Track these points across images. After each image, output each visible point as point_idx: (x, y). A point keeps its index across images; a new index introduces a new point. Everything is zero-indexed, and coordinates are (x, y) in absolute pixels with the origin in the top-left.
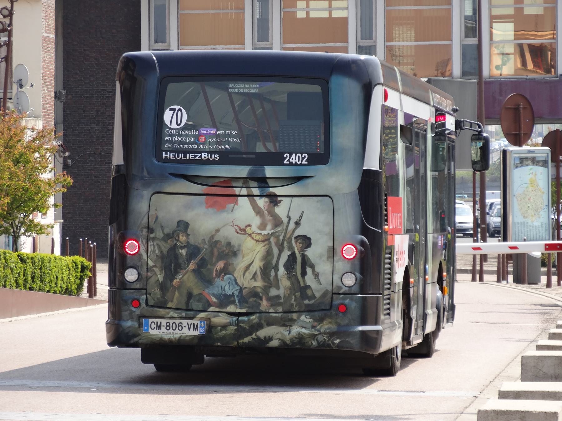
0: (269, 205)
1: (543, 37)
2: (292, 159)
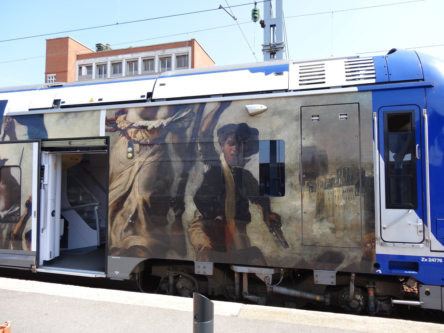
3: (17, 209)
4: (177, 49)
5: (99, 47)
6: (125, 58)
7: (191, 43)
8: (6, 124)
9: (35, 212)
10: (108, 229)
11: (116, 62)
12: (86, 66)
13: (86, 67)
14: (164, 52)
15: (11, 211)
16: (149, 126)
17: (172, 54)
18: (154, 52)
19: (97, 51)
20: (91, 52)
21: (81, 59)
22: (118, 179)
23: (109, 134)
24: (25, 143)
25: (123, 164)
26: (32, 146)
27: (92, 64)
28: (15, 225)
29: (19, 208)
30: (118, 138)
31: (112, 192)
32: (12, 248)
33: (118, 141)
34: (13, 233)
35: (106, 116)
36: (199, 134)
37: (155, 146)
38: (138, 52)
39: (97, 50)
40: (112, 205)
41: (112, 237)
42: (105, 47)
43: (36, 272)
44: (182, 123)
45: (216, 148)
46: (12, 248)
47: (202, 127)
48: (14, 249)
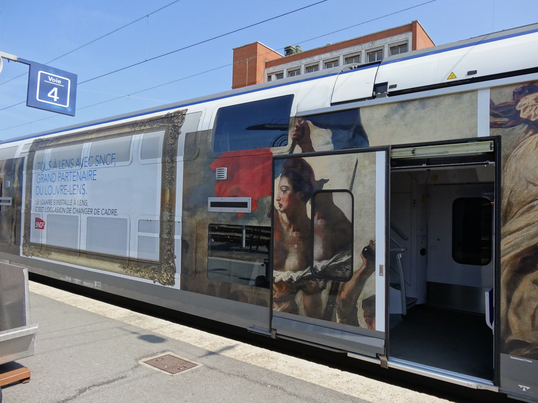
0: (290, 196)
1: (59, 141)
2: (53, 94)
3: (345, 259)
4: (392, 38)
5: (288, 50)
6: (322, 58)
7: (412, 27)
8: (295, 128)
9: (381, 267)
10: (501, 305)
11: (311, 65)
12: (276, 75)
13: (276, 75)
14: (373, 44)
15: (334, 261)
16: (276, 277)
17: (384, 46)
18: (360, 45)
19: (286, 55)
20: (280, 57)
21: (271, 66)
22: (522, 214)
23: (498, 132)
24: (359, 154)
25: (535, 186)
26: (374, 157)
27: (283, 70)
28: (344, 285)
30: (523, 137)
31: (508, 237)
33: (523, 142)
34: (340, 297)
35: (491, 100)
38: (339, 50)
39: (286, 54)
40: (509, 261)
41: (510, 321)
42: (295, 49)
43: (387, 368)
45: (361, 325)
46: (338, 320)
48: (341, 322)
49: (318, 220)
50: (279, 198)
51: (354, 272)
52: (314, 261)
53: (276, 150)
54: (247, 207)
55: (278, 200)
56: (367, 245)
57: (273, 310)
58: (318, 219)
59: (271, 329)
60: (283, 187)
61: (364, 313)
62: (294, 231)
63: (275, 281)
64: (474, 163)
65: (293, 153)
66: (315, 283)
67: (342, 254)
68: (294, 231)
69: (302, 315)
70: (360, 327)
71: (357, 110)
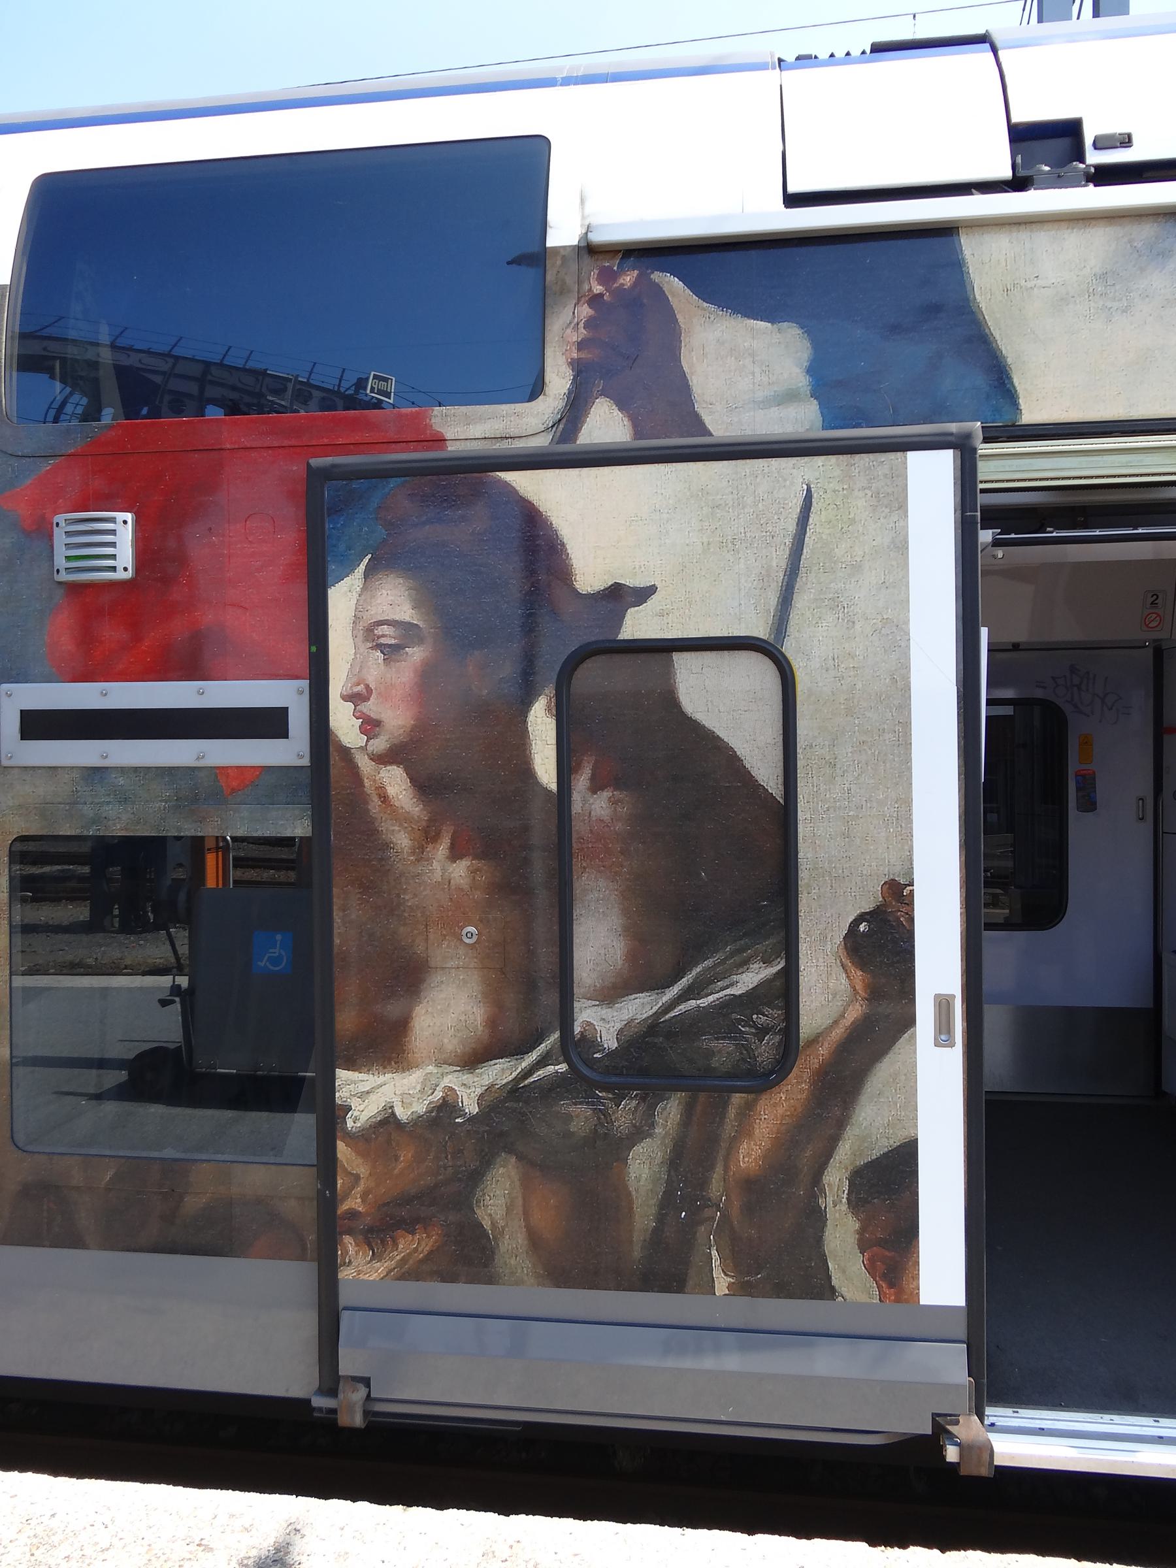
0: (427, 676)
3: (749, 979)
9: (943, 1005)
16: (354, 1103)
24: (819, 461)
26: (899, 478)
28: (749, 1107)
29: (780, 965)
32: (722, 1283)
36: (715, 1187)
37: (401, 1246)
44: (735, 1039)
45: (844, 1290)
46: (722, 1283)
47: (734, 1142)
48: (742, 1288)
49: (594, 792)
50: (358, 684)
51: (801, 1044)
52: (576, 1004)
53: (468, 420)
54: (284, 734)
55: (355, 698)
56: (867, 907)
57: (340, 1276)
58: (596, 786)
59: (331, 1381)
60: (385, 629)
61: (861, 1232)
62: (455, 854)
63: (350, 1124)
64: (1013, 536)
65: (578, 442)
66: (590, 1113)
67: (732, 954)
68: (455, 854)
69: (519, 1282)
70: (840, 1299)
71: (945, 231)
